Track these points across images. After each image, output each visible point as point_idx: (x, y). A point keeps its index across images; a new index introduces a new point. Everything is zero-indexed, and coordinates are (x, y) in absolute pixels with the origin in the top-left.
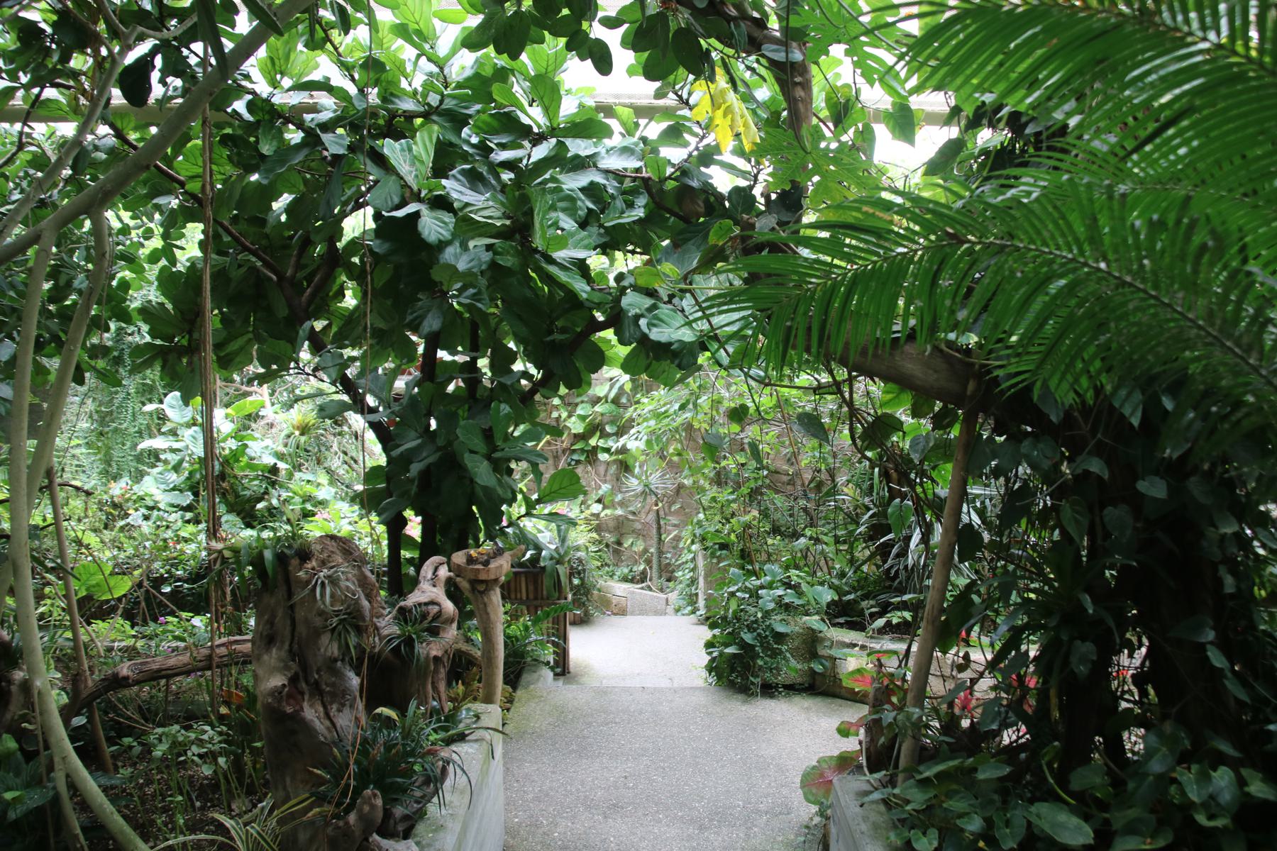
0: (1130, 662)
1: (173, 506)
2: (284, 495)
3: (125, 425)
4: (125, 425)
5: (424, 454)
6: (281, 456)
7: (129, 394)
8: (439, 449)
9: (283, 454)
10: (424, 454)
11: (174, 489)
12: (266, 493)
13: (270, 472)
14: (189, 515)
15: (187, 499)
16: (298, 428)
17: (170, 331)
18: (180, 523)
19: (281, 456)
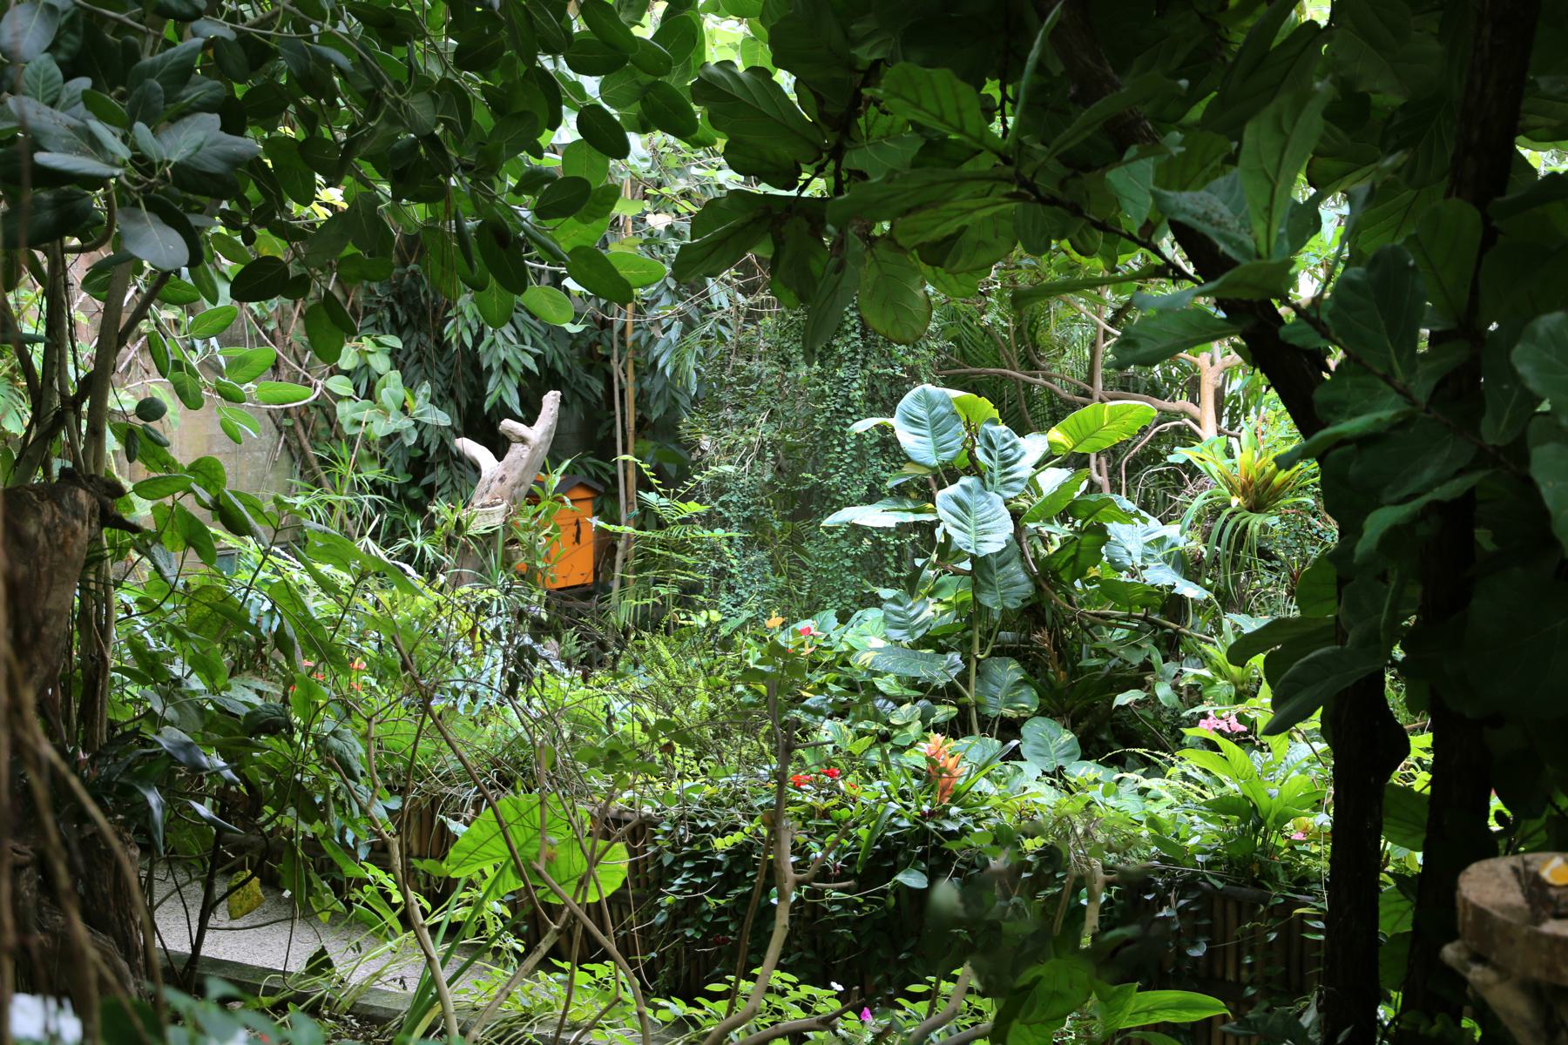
0: (1149, 897)
1: (913, 683)
2: (1191, 673)
3: (837, 479)
4: (837, 479)
5: (1428, 474)
6: (1190, 567)
7: (849, 402)
8: (1483, 458)
9: (1199, 561)
10: (1428, 474)
11: (926, 642)
12: (1147, 666)
13: (1163, 611)
14: (944, 712)
15: (944, 668)
16: (1244, 492)
17: (785, 152)
18: (915, 729)
19: (1190, 567)
